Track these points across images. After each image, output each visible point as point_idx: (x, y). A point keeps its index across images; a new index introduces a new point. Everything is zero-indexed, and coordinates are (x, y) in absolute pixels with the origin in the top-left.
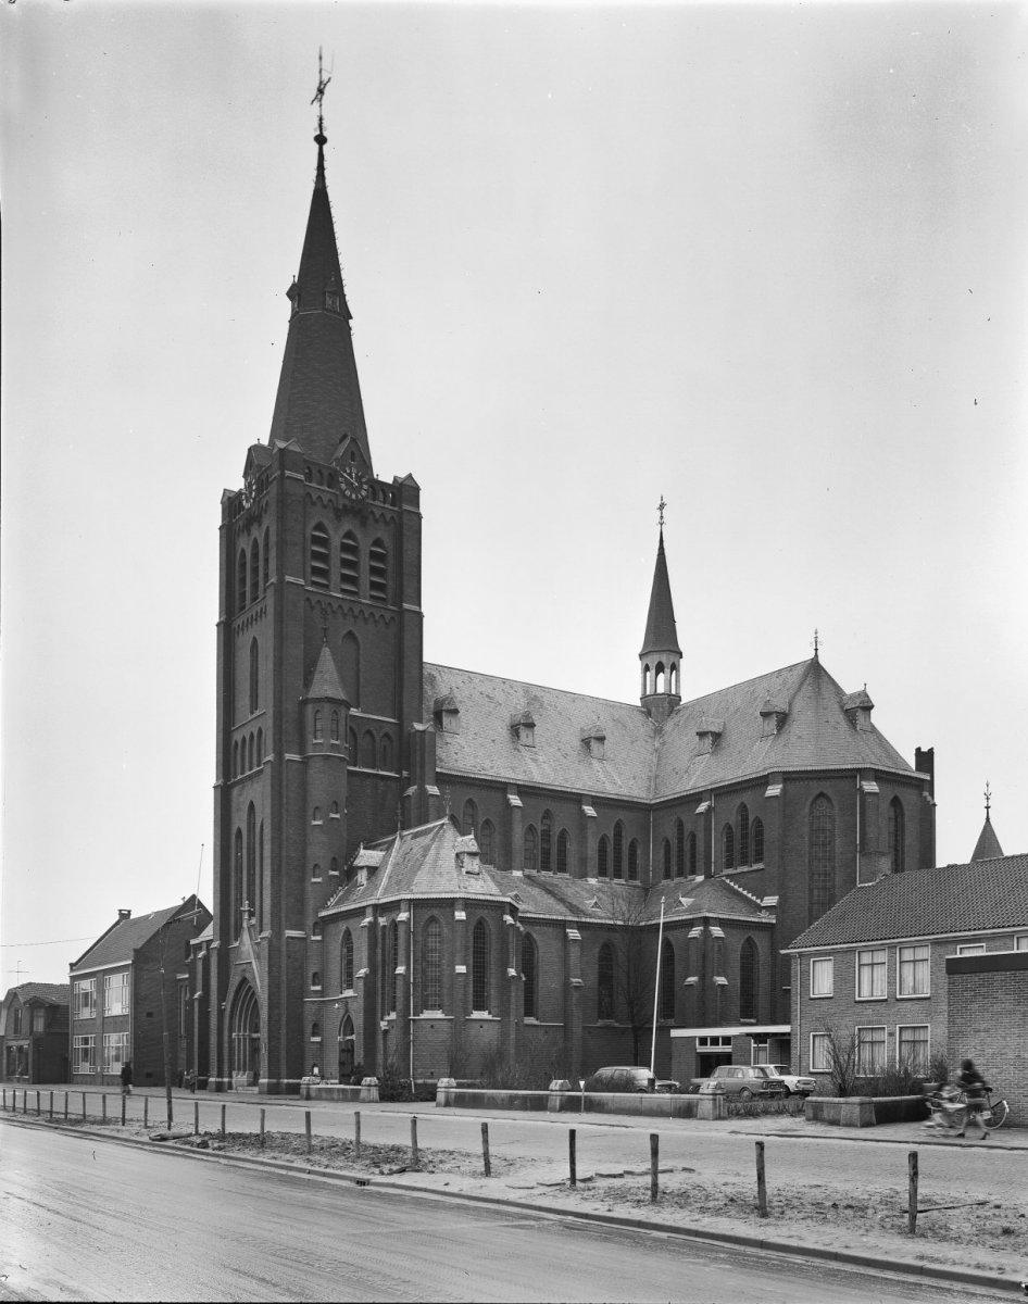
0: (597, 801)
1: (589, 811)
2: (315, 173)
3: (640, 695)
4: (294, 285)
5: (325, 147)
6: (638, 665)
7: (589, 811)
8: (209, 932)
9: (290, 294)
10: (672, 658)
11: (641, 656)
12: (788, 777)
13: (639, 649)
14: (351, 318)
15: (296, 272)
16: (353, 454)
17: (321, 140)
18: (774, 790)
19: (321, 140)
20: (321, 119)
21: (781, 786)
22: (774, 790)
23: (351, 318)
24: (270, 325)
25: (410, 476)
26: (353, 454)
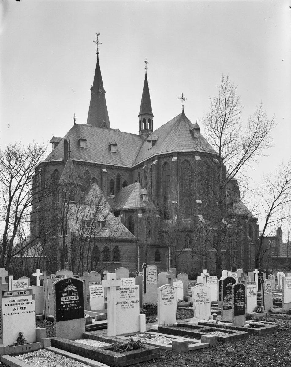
0: (107, 167)
1: (104, 170)
2: (97, 61)
3: (138, 130)
4: (92, 87)
5: (99, 55)
6: (137, 119)
7: (104, 170)
8: (12, 271)
9: (91, 89)
10: (149, 117)
11: (139, 116)
12: (179, 154)
13: (138, 114)
14: (105, 92)
15: (92, 85)
16: (104, 125)
17: (98, 53)
18: (175, 158)
19: (98, 53)
20: (98, 49)
21: (177, 157)
22: (175, 158)
23: (105, 92)
24: (87, 96)
25: (118, 129)
26: (104, 125)
